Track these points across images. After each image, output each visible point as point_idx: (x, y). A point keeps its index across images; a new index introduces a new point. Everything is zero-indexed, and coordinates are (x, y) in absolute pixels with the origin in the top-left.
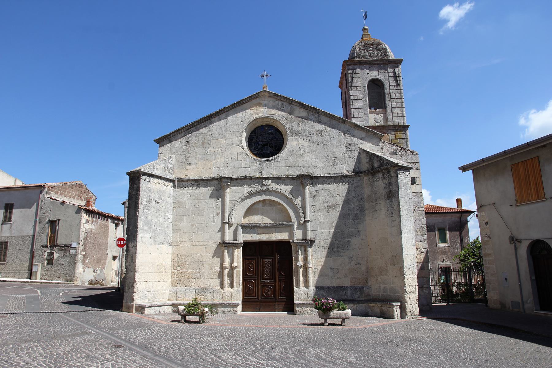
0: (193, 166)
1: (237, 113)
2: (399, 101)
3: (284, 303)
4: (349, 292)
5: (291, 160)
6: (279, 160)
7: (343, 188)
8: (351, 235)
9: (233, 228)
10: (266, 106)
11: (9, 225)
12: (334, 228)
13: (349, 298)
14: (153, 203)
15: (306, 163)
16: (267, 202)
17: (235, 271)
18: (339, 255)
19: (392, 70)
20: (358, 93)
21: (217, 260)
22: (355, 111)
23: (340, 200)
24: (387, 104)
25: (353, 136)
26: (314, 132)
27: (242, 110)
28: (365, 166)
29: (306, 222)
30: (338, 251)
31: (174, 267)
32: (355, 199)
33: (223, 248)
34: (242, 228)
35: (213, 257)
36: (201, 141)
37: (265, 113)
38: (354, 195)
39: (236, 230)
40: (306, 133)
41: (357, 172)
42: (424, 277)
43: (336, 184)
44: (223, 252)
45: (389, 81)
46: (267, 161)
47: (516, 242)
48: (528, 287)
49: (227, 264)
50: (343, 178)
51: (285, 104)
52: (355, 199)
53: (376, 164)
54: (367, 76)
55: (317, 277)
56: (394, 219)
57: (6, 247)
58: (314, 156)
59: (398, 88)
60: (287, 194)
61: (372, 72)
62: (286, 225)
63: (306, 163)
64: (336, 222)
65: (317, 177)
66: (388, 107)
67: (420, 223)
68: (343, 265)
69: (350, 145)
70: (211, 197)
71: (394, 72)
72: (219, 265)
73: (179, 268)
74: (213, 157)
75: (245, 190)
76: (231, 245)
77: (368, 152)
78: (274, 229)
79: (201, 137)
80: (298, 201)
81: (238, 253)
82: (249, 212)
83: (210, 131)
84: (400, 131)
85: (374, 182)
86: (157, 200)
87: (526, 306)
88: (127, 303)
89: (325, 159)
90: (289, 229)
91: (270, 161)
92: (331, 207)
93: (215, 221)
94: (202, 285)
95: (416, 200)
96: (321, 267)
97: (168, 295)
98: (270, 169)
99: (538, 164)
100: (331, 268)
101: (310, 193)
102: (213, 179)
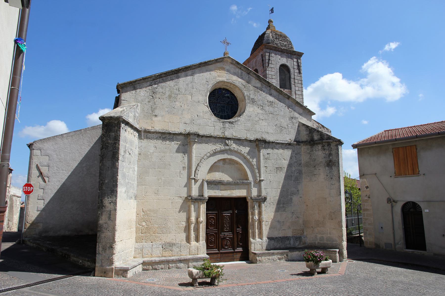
0: (159, 118)
1: (203, 72)
2: (300, 86)
3: (241, 253)
4: (292, 242)
5: (249, 124)
6: (239, 123)
7: (287, 153)
8: (293, 194)
9: (199, 183)
10: (228, 71)
12: (280, 187)
15: (261, 129)
16: (227, 161)
17: (201, 225)
18: (284, 211)
21: (184, 215)
23: (285, 163)
24: (292, 87)
25: (295, 111)
26: (267, 103)
27: (207, 71)
28: (304, 136)
29: (261, 181)
30: (283, 207)
31: (139, 222)
32: (296, 164)
33: (189, 203)
34: (207, 184)
35: (179, 212)
36: (168, 94)
37: (228, 78)
38: (295, 160)
39: (202, 186)
40: (260, 103)
41: (298, 142)
43: (283, 149)
44: (189, 207)
45: (294, 69)
46: (230, 122)
47: (393, 203)
48: (400, 233)
49: (193, 219)
50: (287, 145)
51: (244, 73)
52: (296, 164)
53: (316, 137)
54: (279, 61)
55: (268, 229)
56: (333, 183)
58: (266, 124)
60: (246, 155)
61: (282, 58)
62: (242, 182)
63: (261, 129)
64: (282, 182)
65: (269, 142)
69: (292, 118)
70: (178, 151)
71: (298, 62)
72: (185, 219)
73: (144, 224)
74: (180, 112)
75: (210, 147)
76: (197, 200)
77: (308, 127)
78: (234, 186)
79: (167, 89)
80: (254, 162)
81: (203, 207)
82: (213, 169)
83: (177, 85)
85: (312, 151)
87: (397, 246)
88: (102, 266)
89: (275, 127)
90: (247, 186)
91: (232, 123)
92: (279, 169)
93: (182, 176)
94: (168, 240)
96: (271, 220)
97: (133, 253)
98: (231, 131)
99: (415, 150)
100: (278, 221)
102: (180, 134)
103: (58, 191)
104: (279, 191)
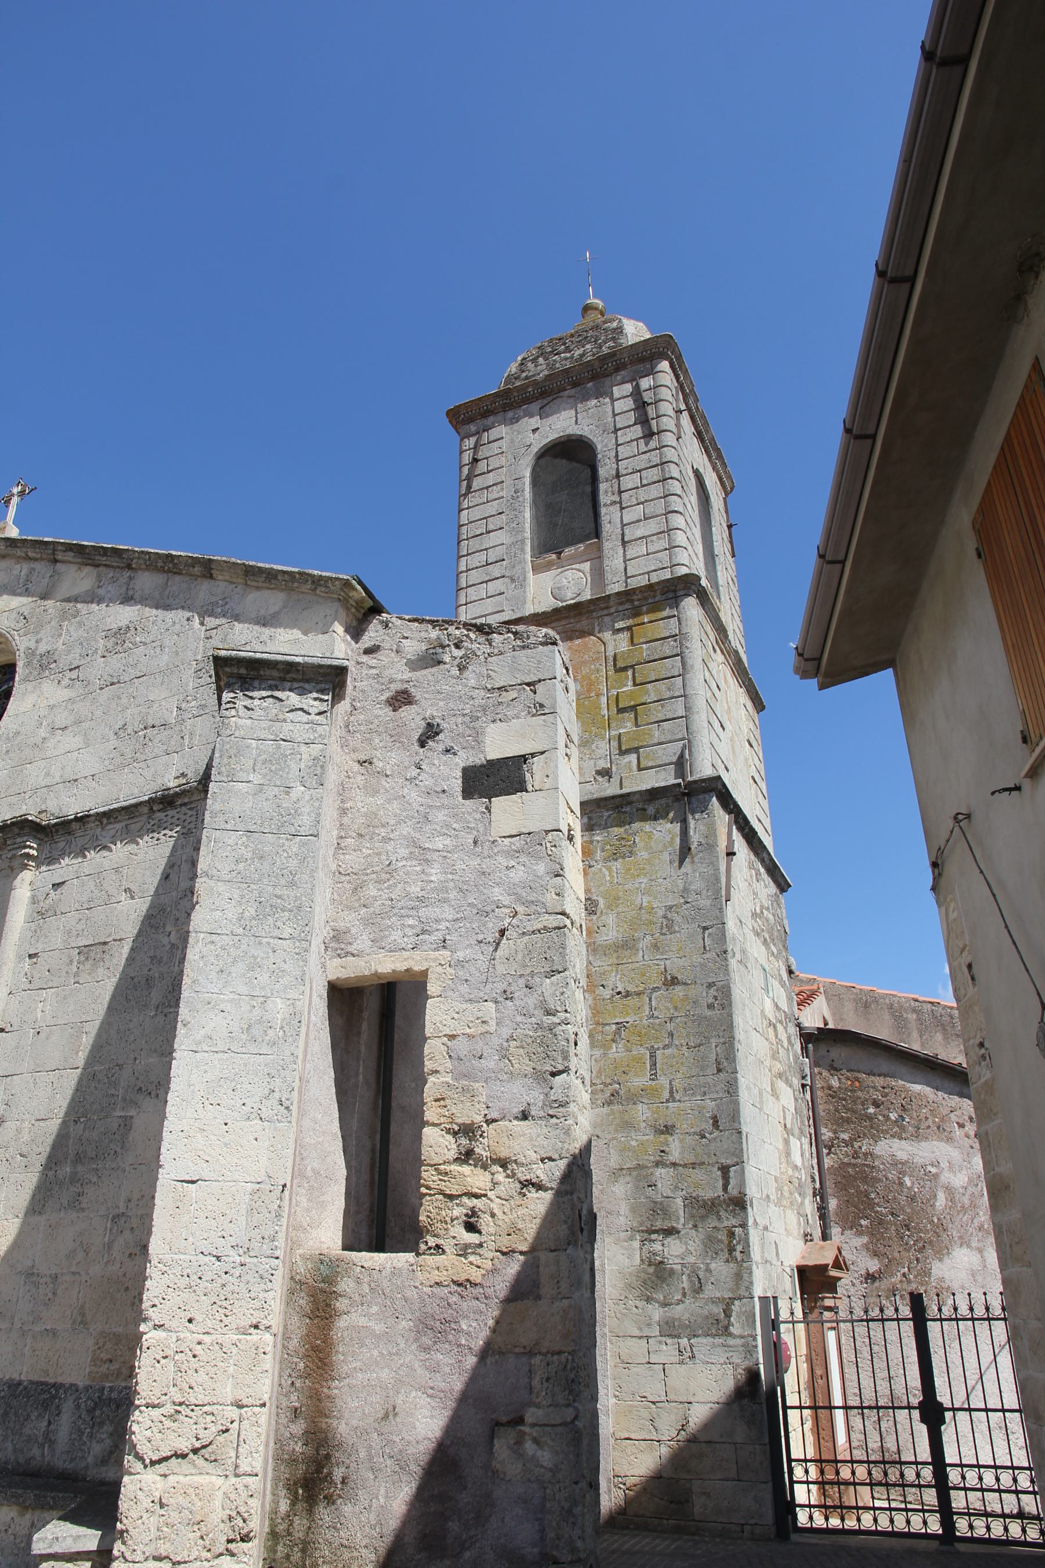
13: (61, 1462)
18: (75, 1204)
19: (628, 388)
20: (492, 508)
22: (475, 576)
25: (237, 618)
42: (530, 1353)
58: (77, 741)
59: (653, 444)
61: (550, 420)
66: (606, 528)
67: (532, 1001)
68: (81, 1255)
71: (637, 394)
84: (656, 608)
89: (114, 742)
95: (518, 875)
101: (34, 900)
103: (599, 1454)
104: (70, 1080)
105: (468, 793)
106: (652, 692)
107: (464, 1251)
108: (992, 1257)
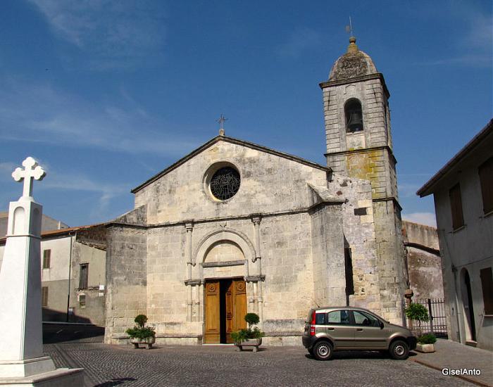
11: (48, 270)
14: (127, 250)
18: (287, 290)
22: (331, 136)
57: (47, 293)
58: (264, 196)
67: (370, 254)
69: (298, 181)
86: (131, 246)
89: (274, 197)
105: (355, 214)
106: (378, 175)
107: (362, 294)
108: (443, 291)
